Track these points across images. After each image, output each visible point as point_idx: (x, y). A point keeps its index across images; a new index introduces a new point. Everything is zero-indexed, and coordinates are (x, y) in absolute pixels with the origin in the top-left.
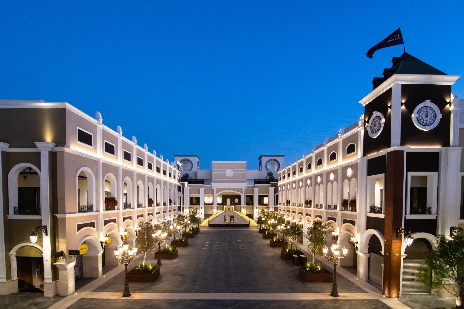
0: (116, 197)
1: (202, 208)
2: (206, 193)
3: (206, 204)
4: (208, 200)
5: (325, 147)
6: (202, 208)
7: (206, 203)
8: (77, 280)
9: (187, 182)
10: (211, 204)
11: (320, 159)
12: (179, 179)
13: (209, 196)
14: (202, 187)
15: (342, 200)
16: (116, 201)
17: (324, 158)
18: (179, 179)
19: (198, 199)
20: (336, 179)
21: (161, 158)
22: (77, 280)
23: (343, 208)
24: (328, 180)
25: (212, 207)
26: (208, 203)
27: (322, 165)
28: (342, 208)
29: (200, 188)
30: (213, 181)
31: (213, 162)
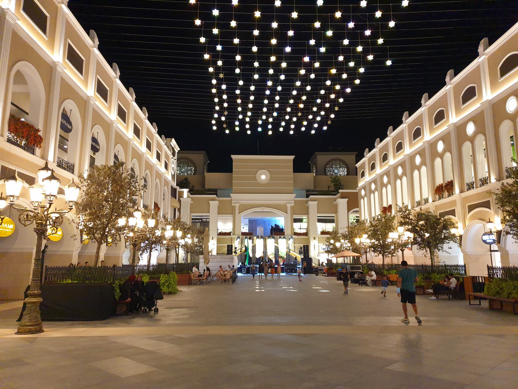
0: (40, 127)
1: (213, 238)
2: (220, 212)
3: (221, 234)
4: (225, 226)
5: (365, 157)
6: (213, 238)
7: (220, 231)
8: (10, 217)
9: (188, 190)
10: (229, 234)
11: (386, 153)
12: (173, 173)
13: (225, 221)
14: (213, 200)
15: (434, 188)
16: (40, 136)
17: (405, 141)
18: (173, 173)
19: (205, 224)
20: (423, 163)
21: (74, 173)
22: (10, 217)
23: (437, 196)
24: (434, 154)
25: (232, 238)
26: (224, 231)
27: (365, 177)
28: (435, 197)
29: (210, 202)
30: (233, 191)
31: (233, 157)
